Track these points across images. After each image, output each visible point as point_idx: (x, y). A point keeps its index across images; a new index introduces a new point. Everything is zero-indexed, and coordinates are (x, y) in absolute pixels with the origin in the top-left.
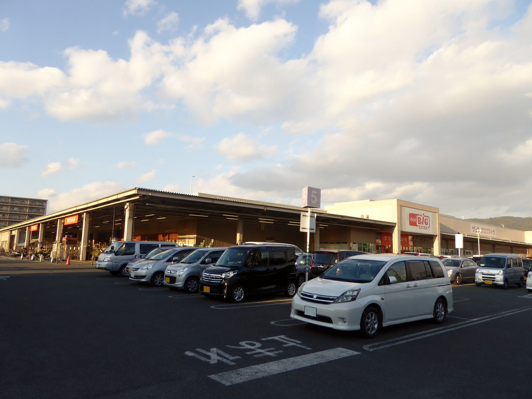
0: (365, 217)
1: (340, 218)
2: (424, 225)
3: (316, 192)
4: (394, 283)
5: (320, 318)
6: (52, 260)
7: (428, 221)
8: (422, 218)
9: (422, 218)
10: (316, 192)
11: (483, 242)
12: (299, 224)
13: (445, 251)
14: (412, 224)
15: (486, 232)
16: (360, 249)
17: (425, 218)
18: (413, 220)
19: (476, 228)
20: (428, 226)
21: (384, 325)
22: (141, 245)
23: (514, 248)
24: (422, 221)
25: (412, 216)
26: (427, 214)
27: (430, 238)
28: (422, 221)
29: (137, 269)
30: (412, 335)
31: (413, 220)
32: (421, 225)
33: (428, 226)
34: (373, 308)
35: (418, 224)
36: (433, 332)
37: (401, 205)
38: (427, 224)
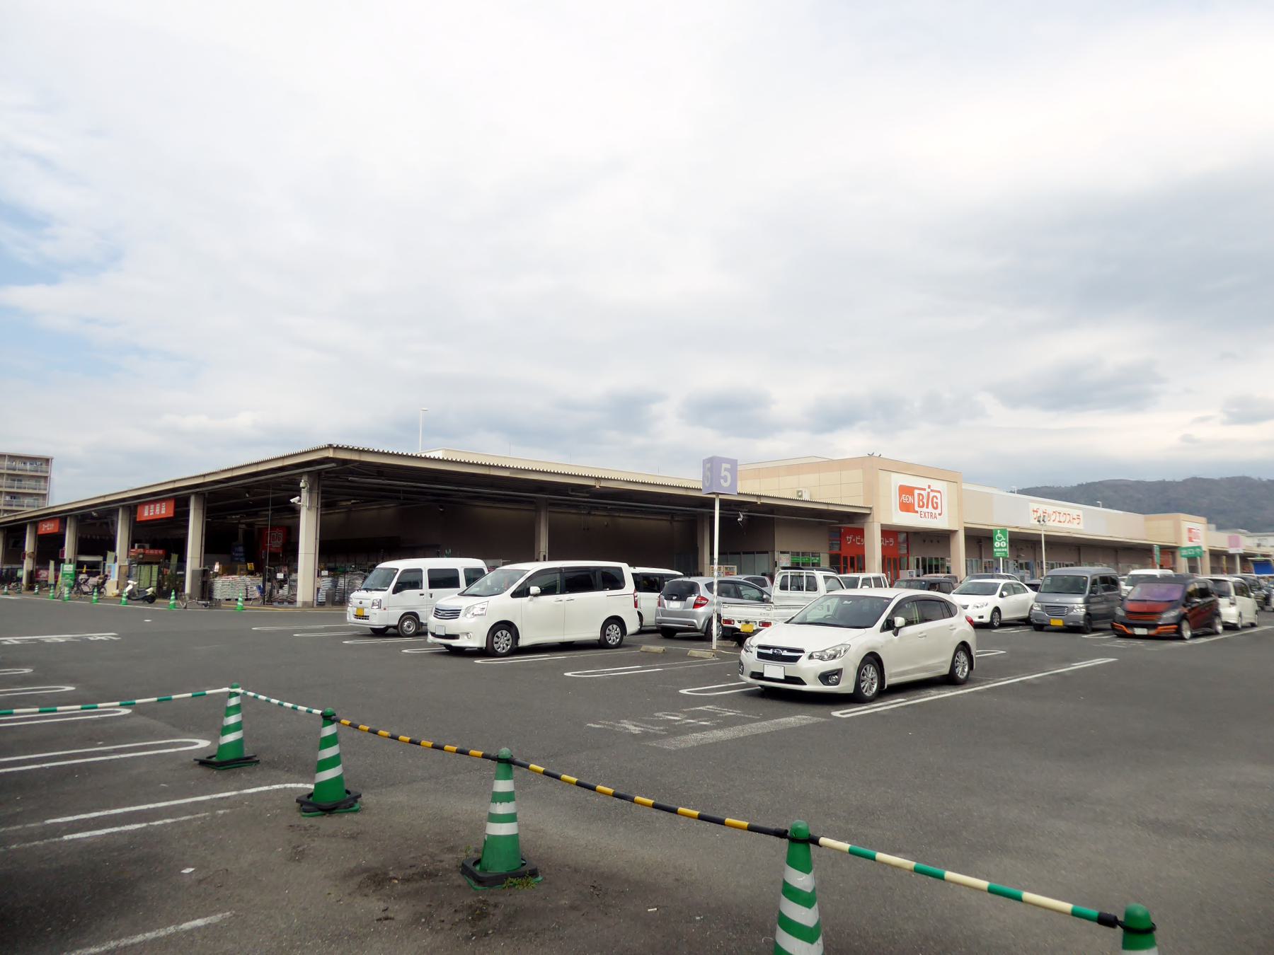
1: (754, 500)
2: (930, 509)
3: (728, 466)
4: (536, 595)
5: (789, 679)
6: (24, 581)
10: (728, 466)
14: (906, 507)
17: (932, 494)
18: (905, 498)
20: (938, 511)
22: (420, 571)
26: (936, 485)
27: (942, 538)
29: (455, 613)
31: (905, 498)
32: (924, 509)
33: (938, 511)
34: (873, 659)
35: (917, 508)
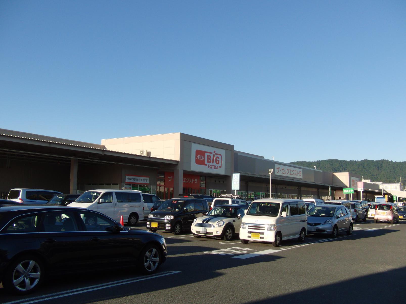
0: (145, 154)
1: (100, 153)
2: (215, 164)
7: (220, 160)
8: (212, 155)
9: (212, 155)
11: (275, 182)
12: (350, 194)
13: (243, 193)
14: (199, 162)
15: (292, 173)
16: (255, 196)
17: (216, 156)
18: (199, 157)
19: (281, 169)
20: (220, 165)
21: (283, 239)
23: (250, 184)
24: (212, 159)
25: (199, 153)
28: (212, 159)
30: (98, 285)
31: (199, 157)
32: (211, 164)
33: (220, 165)
34: (336, 226)
35: (206, 163)
36: (51, 296)
37: (186, 140)
38: (218, 163)
